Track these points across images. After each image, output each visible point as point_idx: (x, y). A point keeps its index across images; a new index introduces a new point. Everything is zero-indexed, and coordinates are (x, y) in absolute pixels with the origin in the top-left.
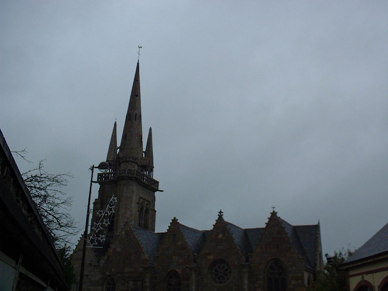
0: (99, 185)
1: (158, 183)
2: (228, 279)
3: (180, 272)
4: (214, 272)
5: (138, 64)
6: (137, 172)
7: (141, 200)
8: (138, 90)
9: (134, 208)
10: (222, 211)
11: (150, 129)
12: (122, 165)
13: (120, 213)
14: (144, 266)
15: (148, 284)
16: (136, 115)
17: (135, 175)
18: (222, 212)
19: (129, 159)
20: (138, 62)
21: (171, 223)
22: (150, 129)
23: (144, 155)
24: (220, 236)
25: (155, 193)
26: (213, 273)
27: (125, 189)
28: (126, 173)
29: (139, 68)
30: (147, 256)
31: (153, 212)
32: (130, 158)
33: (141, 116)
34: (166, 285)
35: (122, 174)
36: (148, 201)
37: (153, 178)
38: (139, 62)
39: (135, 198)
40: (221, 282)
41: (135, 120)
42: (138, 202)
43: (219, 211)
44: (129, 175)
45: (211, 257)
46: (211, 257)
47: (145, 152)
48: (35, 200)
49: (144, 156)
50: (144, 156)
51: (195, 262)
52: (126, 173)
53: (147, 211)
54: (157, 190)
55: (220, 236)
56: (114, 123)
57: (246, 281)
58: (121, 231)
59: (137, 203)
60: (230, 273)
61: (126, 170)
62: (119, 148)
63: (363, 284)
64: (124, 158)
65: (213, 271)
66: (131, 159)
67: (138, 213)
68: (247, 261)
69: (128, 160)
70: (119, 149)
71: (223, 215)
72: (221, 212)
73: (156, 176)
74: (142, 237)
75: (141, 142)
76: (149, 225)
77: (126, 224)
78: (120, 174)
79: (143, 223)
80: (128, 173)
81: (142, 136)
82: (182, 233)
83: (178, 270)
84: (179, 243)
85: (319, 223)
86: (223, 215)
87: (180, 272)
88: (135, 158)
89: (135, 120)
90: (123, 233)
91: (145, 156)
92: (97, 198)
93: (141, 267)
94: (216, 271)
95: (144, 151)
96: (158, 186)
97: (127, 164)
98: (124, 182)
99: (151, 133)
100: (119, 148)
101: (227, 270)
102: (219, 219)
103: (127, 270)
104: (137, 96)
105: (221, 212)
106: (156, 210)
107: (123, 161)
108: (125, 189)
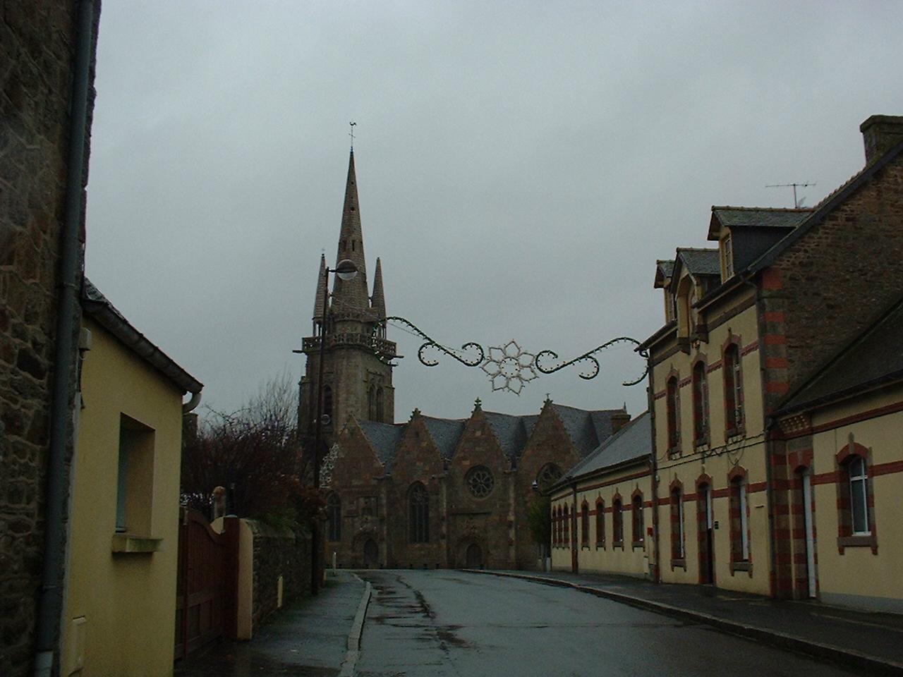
0: (306, 356)
2: (490, 491)
5: (352, 153)
7: (371, 376)
8: (354, 199)
9: (360, 389)
10: (480, 399)
11: (378, 261)
12: (339, 327)
13: (340, 399)
14: (378, 477)
15: (384, 501)
16: (353, 241)
17: (358, 342)
21: (411, 417)
22: (378, 261)
23: (370, 303)
24: (478, 433)
26: (470, 484)
27: (345, 363)
28: (345, 340)
29: (354, 173)
30: (381, 463)
31: (389, 390)
33: (362, 243)
34: (408, 501)
36: (380, 375)
39: (361, 375)
40: (481, 496)
43: (476, 399)
44: (350, 343)
45: (466, 463)
46: (466, 463)
47: (372, 299)
49: (370, 306)
50: (370, 306)
51: (445, 469)
52: (345, 340)
53: (380, 390)
55: (478, 433)
56: (321, 255)
57: (512, 495)
58: (344, 429)
59: (365, 381)
60: (493, 483)
61: (345, 335)
62: (331, 295)
63: (851, 452)
64: (340, 317)
65: (471, 482)
66: (351, 318)
67: (366, 396)
68: (514, 466)
69: (346, 318)
70: (331, 298)
71: (480, 405)
72: (478, 401)
74: (376, 437)
75: (365, 283)
76: (385, 411)
77: (350, 419)
79: (375, 409)
80: (348, 340)
81: (365, 274)
82: (427, 431)
83: (423, 481)
84: (424, 444)
85: (625, 407)
86: (480, 405)
90: (346, 431)
91: (372, 306)
92: (304, 375)
93: (374, 479)
94: (474, 480)
97: (346, 325)
98: (342, 354)
99: (381, 282)
100: (331, 295)
101: (488, 479)
102: (475, 410)
103: (355, 482)
104: (353, 209)
105: (478, 401)
106: (394, 386)
107: (340, 321)
108: (345, 363)
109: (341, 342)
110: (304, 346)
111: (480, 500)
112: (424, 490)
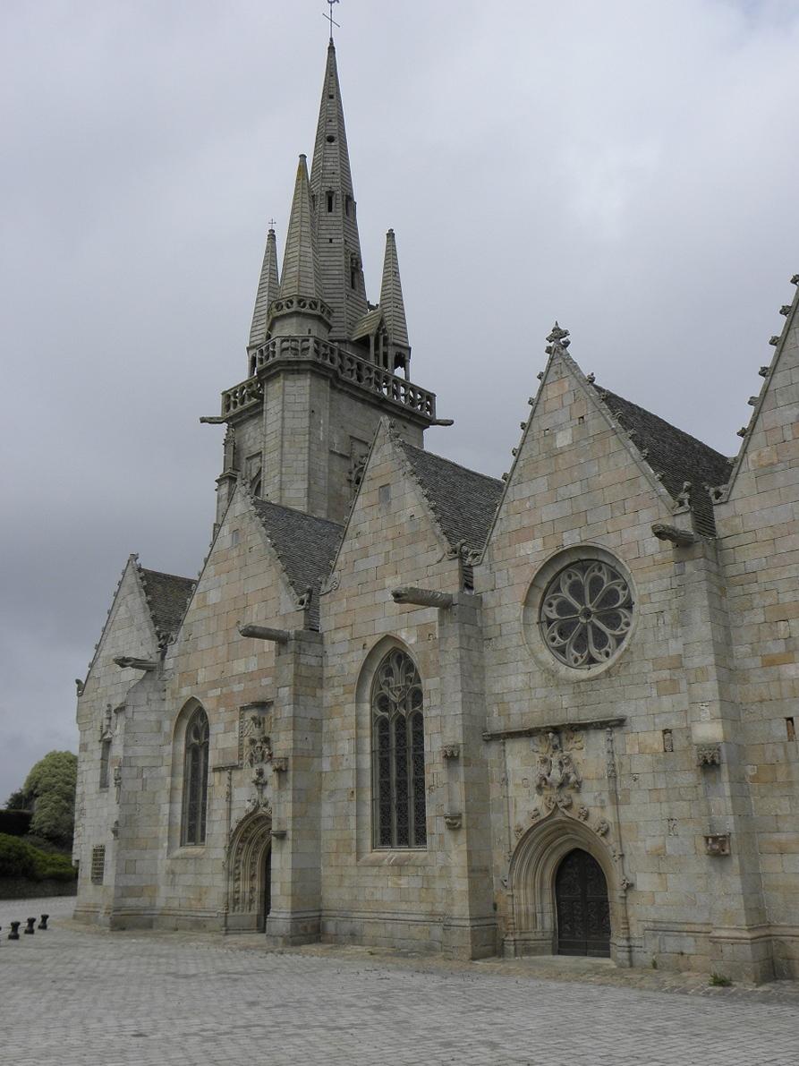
1: (430, 397)
3: (412, 641)
4: (554, 615)
6: (316, 342)
18: (566, 334)
19: (288, 307)
20: (331, 43)
25: (425, 431)
32: (292, 302)
35: (267, 358)
37: (411, 381)
38: (335, 45)
40: (592, 660)
41: (330, 210)
42: (344, 453)
48: (541, 692)
54: (431, 422)
60: (629, 605)
73: (420, 372)
78: (261, 360)
83: (403, 635)
86: (567, 344)
87: (412, 641)
88: (308, 302)
89: (330, 210)
95: (373, 303)
96: (431, 409)
109: (271, 359)
110: (227, 407)
111: (584, 674)
112: (410, 667)
